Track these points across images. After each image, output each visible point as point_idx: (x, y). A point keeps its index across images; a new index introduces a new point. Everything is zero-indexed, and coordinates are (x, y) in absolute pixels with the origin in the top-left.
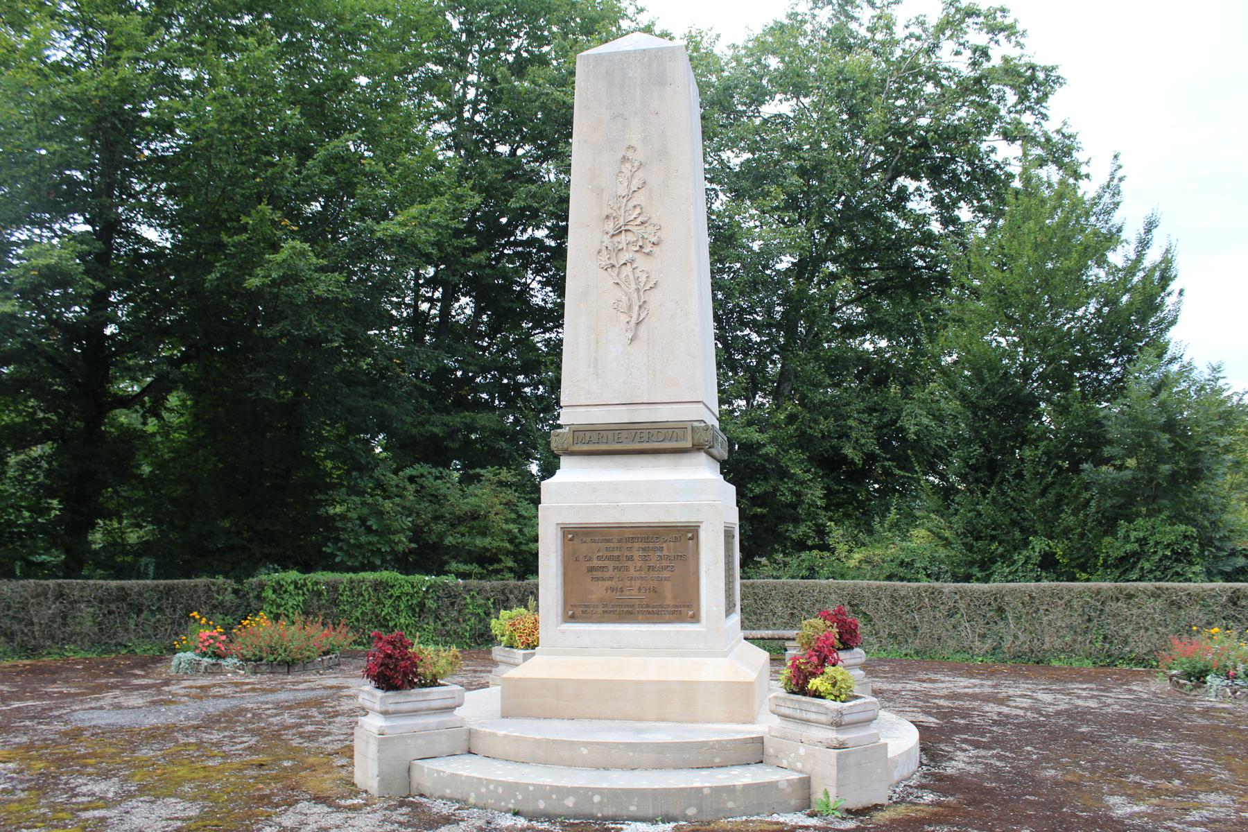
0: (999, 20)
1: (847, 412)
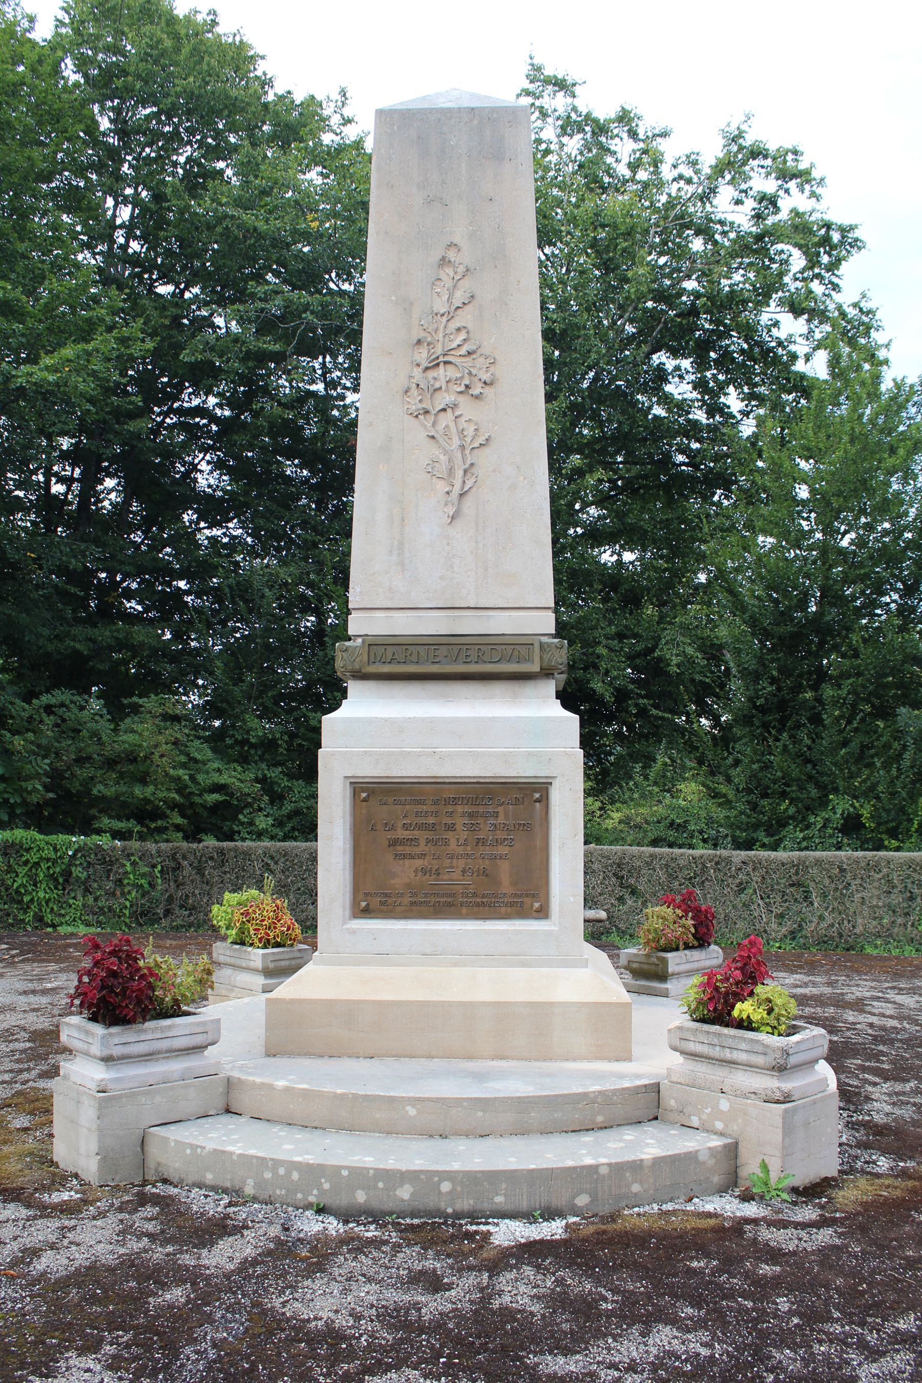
1: (595, 638)
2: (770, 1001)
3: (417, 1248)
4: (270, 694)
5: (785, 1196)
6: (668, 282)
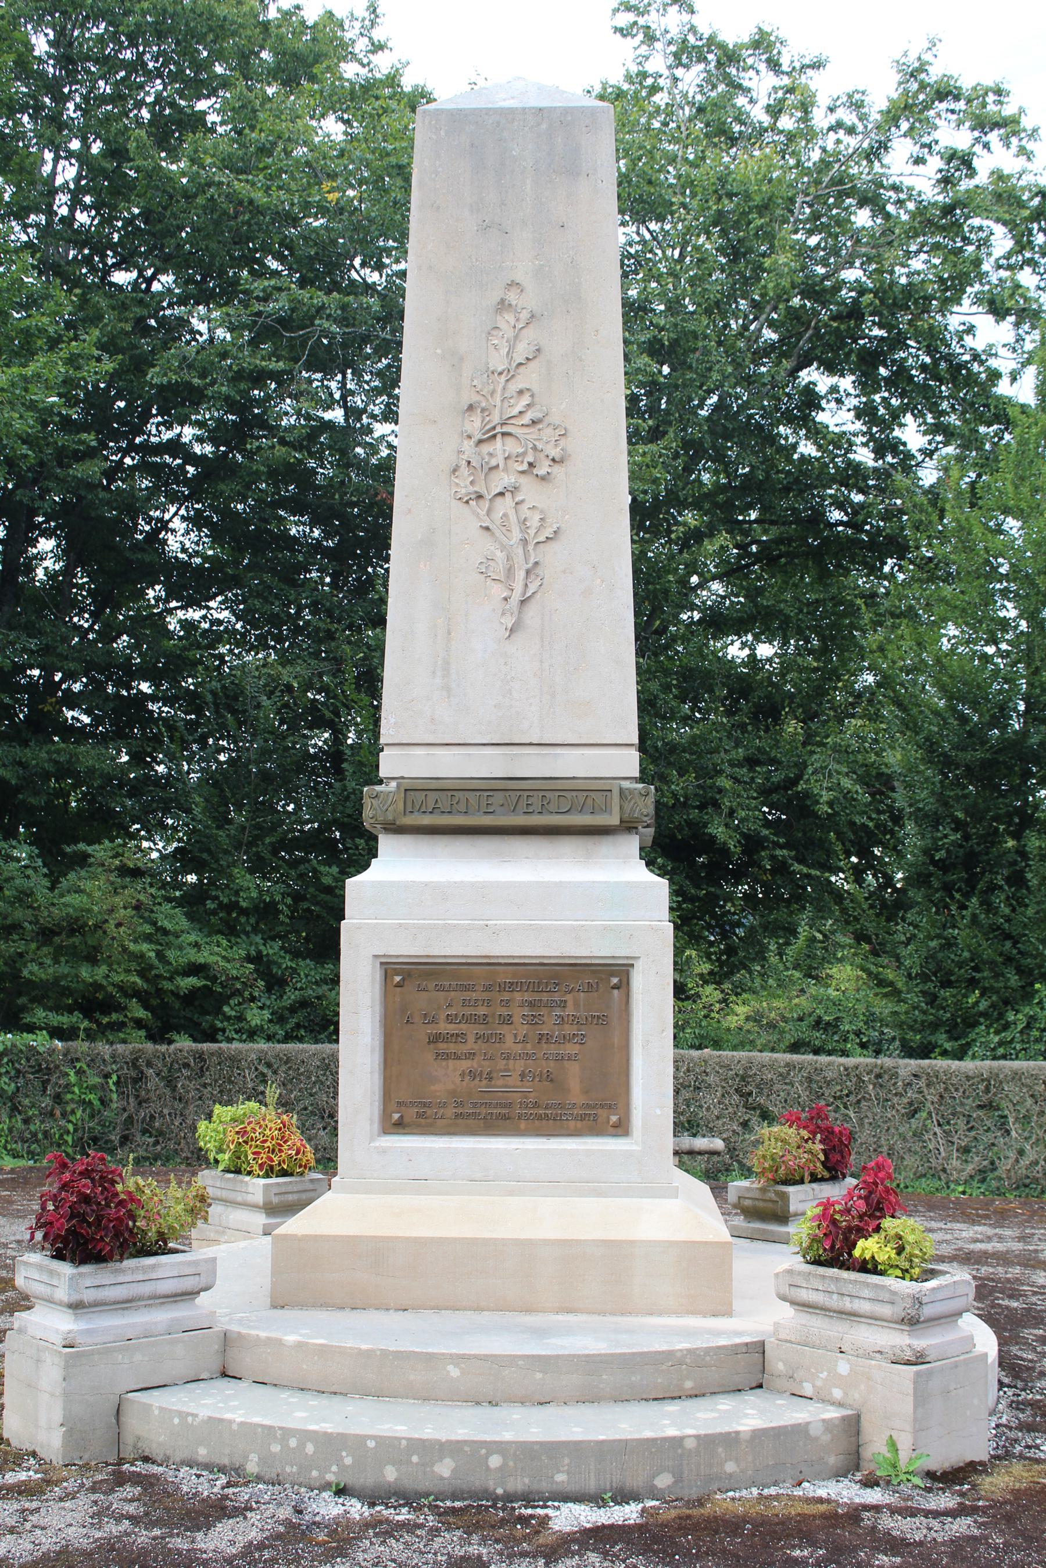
0: (991, 108)
1: (715, 765)
2: (900, 1238)
3: (459, 1533)
4: (268, 840)
5: (917, 1481)
6: (821, 270)
